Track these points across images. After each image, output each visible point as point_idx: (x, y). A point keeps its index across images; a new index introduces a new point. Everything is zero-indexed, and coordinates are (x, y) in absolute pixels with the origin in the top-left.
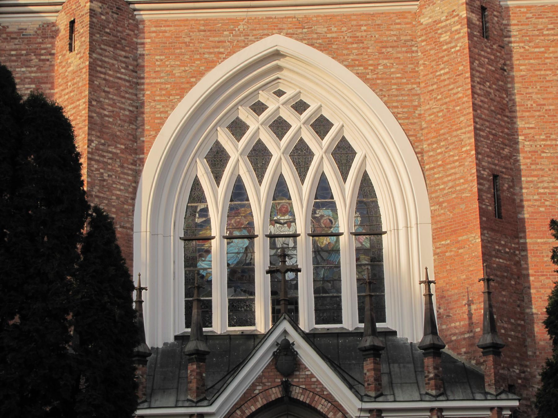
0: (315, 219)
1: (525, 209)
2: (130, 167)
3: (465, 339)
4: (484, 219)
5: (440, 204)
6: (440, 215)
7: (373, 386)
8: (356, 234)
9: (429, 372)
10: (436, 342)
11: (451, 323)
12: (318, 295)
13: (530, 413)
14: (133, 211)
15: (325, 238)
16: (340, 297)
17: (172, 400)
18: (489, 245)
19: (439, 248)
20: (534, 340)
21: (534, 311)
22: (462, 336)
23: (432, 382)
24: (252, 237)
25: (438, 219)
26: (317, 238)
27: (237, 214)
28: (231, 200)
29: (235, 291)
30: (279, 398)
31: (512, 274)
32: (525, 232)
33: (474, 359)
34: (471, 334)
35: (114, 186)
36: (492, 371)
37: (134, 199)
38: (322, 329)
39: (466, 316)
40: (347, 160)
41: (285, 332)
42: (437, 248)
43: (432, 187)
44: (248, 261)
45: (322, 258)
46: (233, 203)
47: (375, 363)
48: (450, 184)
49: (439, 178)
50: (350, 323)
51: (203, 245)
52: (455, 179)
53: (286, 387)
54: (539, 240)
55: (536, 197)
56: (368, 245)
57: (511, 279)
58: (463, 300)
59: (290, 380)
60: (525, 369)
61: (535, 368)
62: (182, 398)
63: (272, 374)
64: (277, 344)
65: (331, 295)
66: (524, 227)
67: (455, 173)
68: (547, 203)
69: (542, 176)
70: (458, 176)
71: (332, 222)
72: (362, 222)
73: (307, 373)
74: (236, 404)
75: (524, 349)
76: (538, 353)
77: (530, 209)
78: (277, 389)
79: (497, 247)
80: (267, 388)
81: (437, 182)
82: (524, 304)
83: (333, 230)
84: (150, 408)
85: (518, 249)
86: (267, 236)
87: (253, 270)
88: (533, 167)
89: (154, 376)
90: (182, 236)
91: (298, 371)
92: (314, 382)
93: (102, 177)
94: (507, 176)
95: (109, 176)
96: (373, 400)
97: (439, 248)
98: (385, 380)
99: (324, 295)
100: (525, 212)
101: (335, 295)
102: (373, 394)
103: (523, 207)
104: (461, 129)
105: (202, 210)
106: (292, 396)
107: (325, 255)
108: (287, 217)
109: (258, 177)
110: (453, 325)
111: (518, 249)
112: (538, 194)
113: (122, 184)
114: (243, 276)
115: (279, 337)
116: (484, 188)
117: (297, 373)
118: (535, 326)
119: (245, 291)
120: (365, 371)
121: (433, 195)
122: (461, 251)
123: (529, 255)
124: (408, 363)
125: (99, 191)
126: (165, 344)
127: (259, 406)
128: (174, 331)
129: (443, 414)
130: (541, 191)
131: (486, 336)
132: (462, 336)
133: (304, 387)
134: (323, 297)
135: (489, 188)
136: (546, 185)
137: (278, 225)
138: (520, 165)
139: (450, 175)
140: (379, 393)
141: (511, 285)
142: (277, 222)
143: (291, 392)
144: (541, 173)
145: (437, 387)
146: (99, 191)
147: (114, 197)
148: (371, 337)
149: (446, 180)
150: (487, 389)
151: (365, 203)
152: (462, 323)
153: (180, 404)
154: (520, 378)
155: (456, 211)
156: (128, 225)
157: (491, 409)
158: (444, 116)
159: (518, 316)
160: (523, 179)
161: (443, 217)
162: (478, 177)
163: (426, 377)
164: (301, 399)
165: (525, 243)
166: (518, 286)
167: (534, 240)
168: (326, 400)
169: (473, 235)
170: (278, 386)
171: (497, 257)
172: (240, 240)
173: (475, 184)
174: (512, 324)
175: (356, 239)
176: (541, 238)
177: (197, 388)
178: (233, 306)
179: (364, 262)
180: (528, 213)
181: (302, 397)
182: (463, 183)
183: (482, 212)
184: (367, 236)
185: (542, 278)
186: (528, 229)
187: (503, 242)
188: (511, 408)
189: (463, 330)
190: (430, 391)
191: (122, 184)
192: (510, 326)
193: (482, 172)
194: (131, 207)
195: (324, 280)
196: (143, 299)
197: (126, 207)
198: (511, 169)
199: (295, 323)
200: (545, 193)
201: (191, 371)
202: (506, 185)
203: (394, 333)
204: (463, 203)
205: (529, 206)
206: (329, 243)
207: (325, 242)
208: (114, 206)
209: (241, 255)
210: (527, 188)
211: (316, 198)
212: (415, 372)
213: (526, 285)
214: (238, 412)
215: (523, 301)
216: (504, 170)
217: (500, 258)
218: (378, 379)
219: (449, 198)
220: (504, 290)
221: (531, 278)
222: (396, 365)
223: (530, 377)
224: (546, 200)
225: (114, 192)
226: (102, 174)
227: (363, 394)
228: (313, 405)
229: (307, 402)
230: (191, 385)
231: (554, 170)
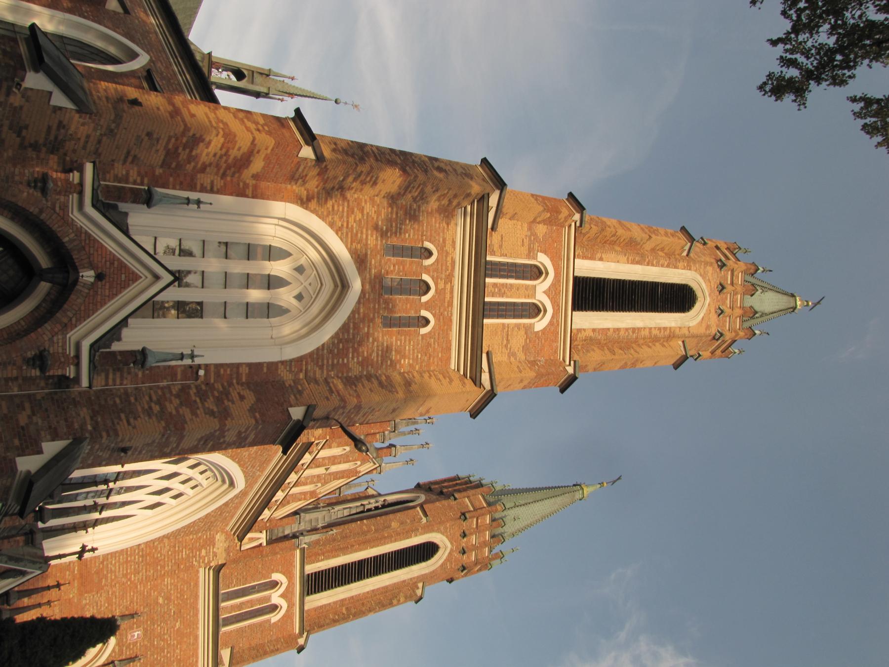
5: (102, 563)
67: (119, 571)
104: (146, 572)
158: (157, 558)
161: (93, 565)
169: (76, 592)
219: (105, 569)
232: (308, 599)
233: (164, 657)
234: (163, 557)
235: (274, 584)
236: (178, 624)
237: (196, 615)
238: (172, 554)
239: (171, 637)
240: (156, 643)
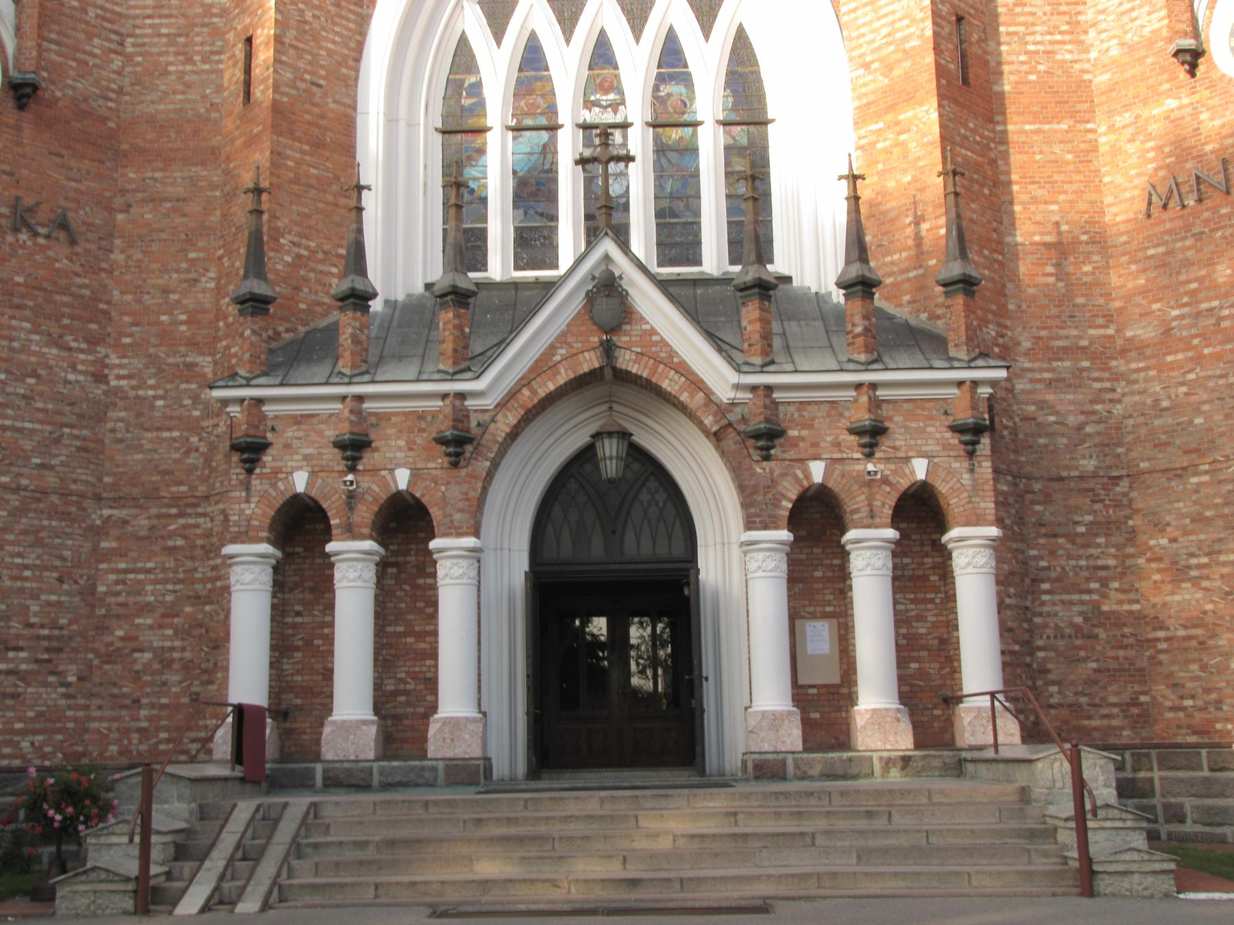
0: (658, 100)
1: (1005, 76)
2: (352, 7)
3: (908, 280)
4: (943, 82)
5: (867, 66)
6: (865, 85)
7: (759, 346)
8: (725, 124)
9: (854, 325)
10: (867, 274)
11: (884, 256)
12: (662, 221)
13: (1012, 401)
14: (357, 79)
15: (674, 130)
16: (698, 224)
17: (412, 373)
18: (951, 125)
19: (864, 137)
20: (1018, 286)
21: (1019, 239)
22: (904, 276)
23: (860, 340)
24: (553, 128)
25: (864, 90)
26: (660, 130)
27: (530, 92)
28: (520, 70)
29: (526, 213)
30: (595, 369)
31: (985, 178)
32: (1004, 113)
33: (924, 311)
34: (921, 271)
35: (324, 34)
36: (962, 321)
37: (358, 60)
38: (668, 274)
39: (910, 242)
40: (711, 7)
41: (607, 258)
42: (860, 138)
43: (851, 40)
44: (547, 167)
45: (669, 161)
46: (522, 74)
47: (761, 309)
48: (885, 31)
49: (864, 25)
50: (715, 263)
51: (473, 142)
52: (894, 22)
53: (608, 349)
54: (1027, 127)
55: (1023, 58)
56: (744, 141)
57: (983, 186)
58: (907, 216)
59: (615, 339)
60: (1004, 331)
61: (1020, 330)
62: (430, 367)
63: (583, 328)
64: (594, 278)
65: (683, 220)
66: (1003, 104)
67: (893, 12)
68: (1041, 68)
69: (1033, 24)
70: (898, 15)
71: (685, 105)
72: (734, 104)
73: (645, 327)
74: (522, 379)
75: (1003, 300)
76: (1024, 307)
77: (1012, 78)
78: (592, 353)
79: (963, 131)
80: (575, 351)
81: (862, 31)
82: (1002, 229)
83: (687, 118)
84: (373, 382)
85: (993, 140)
86: (579, 126)
87: (555, 180)
88: (1018, 10)
89: (385, 340)
90: (440, 125)
91: (629, 323)
92: (657, 342)
93: (303, 16)
94: (976, 22)
95: (314, 16)
96: (759, 369)
97: (864, 137)
98: (777, 342)
99: (672, 220)
100: (1005, 82)
101: (690, 220)
102: (758, 360)
103: (1001, 73)
105: (471, 85)
106: (618, 366)
107: (673, 156)
108: (611, 96)
109: (564, 32)
110: (888, 259)
111: (993, 140)
112: (1026, 53)
113: (337, 33)
114: (538, 190)
115: (595, 267)
116: (943, 33)
117: (627, 327)
118: (1021, 263)
119: (541, 215)
120: (744, 323)
121: (856, 53)
122: (903, 137)
123: (1011, 151)
124: (814, 320)
125: (296, 38)
126: (409, 296)
127: (561, 380)
128: (425, 275)
129: (878, 393)
130: (1031, 48)
131: (951, 264)
132: (904, 276)
133: (639, 350)
134: (669, 223)
135: (950, 34)
136: (1038, 38)
137: (597, 109)
138: (996, 7)
139: (885, 15)
140: (768, 359)
141: (984, 195)
142: (596, 104)
143: (617, 358)
144: (1030, 19)
145: (868, 349)
146: (296, 38)
147: (323, 53)
148: (756, 266)
149: (876, 25)
150: (952, 353)
151: (741, 75)
152: (904, 255)
153: (425, 377)
154: (997, 345)
155: (896, 72)
156: (347, 101)
157: (960, 384)
159: (994, 246)
160: (1002, 29)
161: (871, 87)
162: (933, 12)
163: (848, 333)
164: (634, 371)
165: (1005, 132)
166: (994, 199)
167: (1019, 127)
168: (676, 372)
170: (594, 349)
171: (962, 147)
172: (534, 133)
173: (929, 24)
174: (985, 257)
175: (725, 132)
176: (1032, 123)
177: (455, 351)
178: (522, 237)
179: (738, 168)
180: (1009, 83)
181: (636, 366)
182: (908, 26)
183: (941, 71)
184: (744, 127)
185: (1032, 187)
186: (1011, 109)
187: (971, 125)
188: (993, 383)
189: (904, 266)
190: (855, 357)
191: (337, 33)
192: (982, 260)
193: (940, 6)
194: (353, 73)
195: (672, 197)
196: (364, 204)
197: (344, 70)
198: (983, 13)
199: (624, 245)
200: (1037, 52)
201: (445, 324)
202: (975, 36)
203: (787, 279)
204: (907, 59)
205: (1011, 73)
206: (681, 138)
207: (674, 136)
208: (322, 67)
209: (536, 156)
210: (1009, 44)
211: (659, 66)
212: (827, 332)
213: (1007, 198)
214: (526, 392)
215: (1001, 223)
216: (972, 11)
217: (967, 149)
218: (767, 337)
220: (973, 201)
221: (1015, 188)
222: (793, 323)
223: (1011, 345)
224: (1039, 63)
225: (325, 44)
226: (302, 11)
227: (740, 362)
228: (654, 380)
229: (645, 375)
230: (444, 346)
231: (1052, 14)
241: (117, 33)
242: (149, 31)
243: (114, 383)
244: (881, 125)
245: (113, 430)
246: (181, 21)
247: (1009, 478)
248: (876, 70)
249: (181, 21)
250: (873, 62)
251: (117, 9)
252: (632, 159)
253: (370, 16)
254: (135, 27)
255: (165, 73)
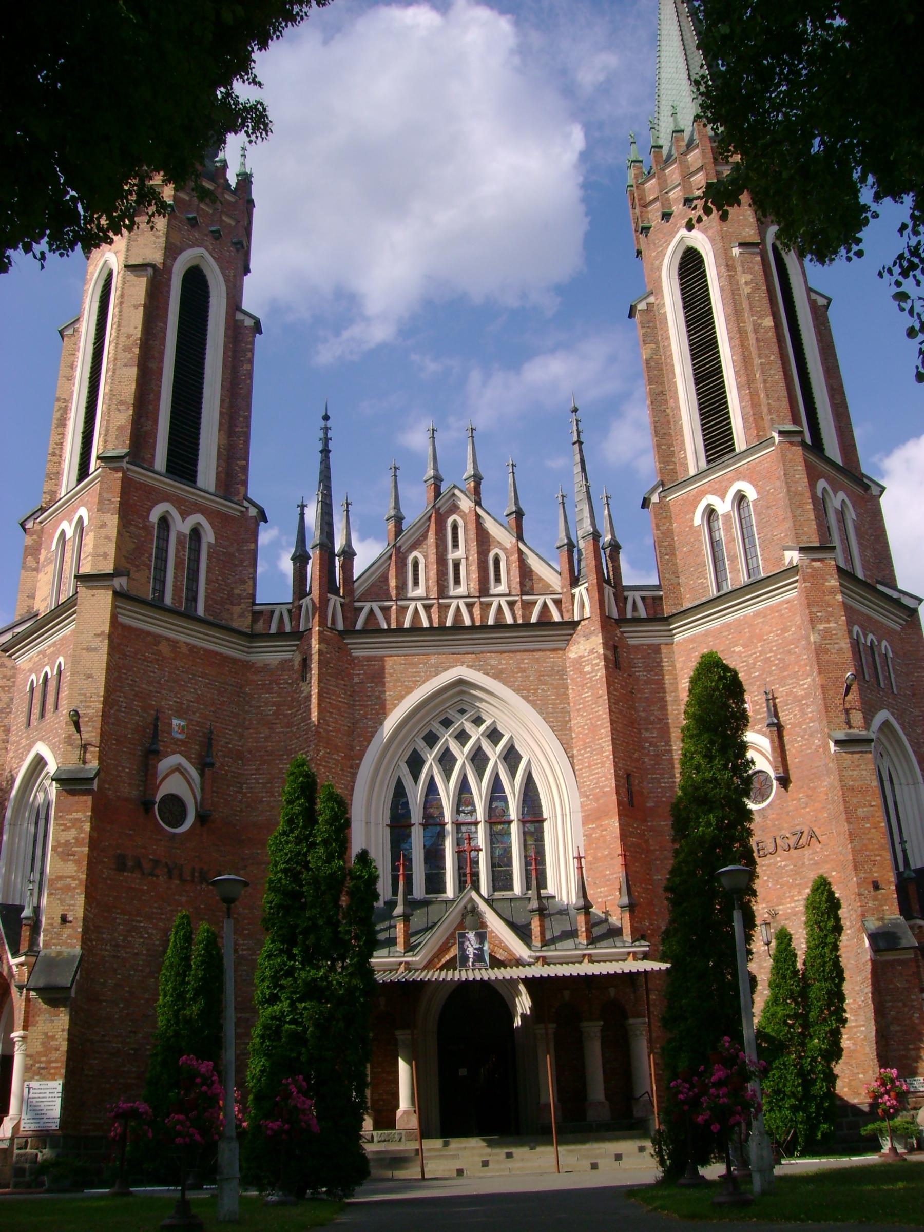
5: (587, 797)
42: (585, 831)
55: (659, 790)
68: (668, 794)
88: (657, 767)
108: (470, 808)
136: (666, 780)
174: (643, 888)
183: (619, 803)
199: (478, 890)
232: (201, 482)
233: (775, 655)
234: (588, 721)
235: (164, 522)
236: (737, 649)
237: (727, 626)
238: (586, 711)
239: (751, 655)
240: (757, 674)
241: (239, 783)
242: (253, 781)
243: (240, 953)
244: (594, 826)
245: (241, 976)
246: (269, 776)
247: (656, 992)
248: (592, 799)
249: (269, 776)
250: (590, 795)
251: (240, 771)
252: (481, 850)
253: (356, 773)
254: (247, 779)
255: (262, 801)
